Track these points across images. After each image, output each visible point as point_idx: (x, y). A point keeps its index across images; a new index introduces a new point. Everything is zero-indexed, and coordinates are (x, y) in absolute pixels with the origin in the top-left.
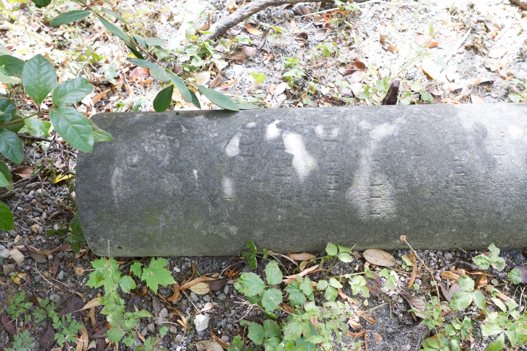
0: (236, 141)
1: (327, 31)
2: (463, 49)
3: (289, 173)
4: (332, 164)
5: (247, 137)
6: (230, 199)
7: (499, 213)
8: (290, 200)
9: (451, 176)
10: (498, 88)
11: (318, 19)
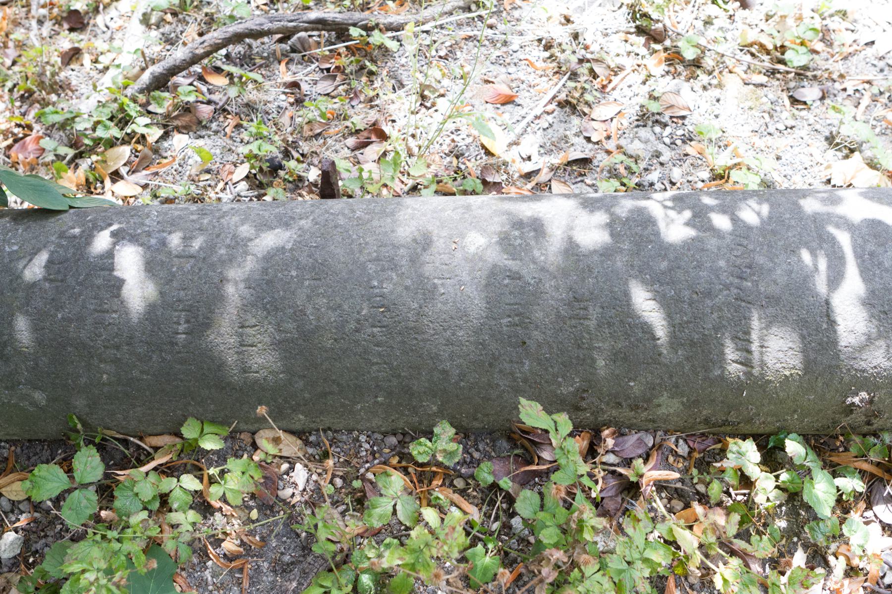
0: (43, 257)
2: (553, 106)
3: (115, 308)
4: (182, 293)
5: (61, 251)
6: (27, 348)
7: (445, 372)
8: (118, 350)
10: (598, 169)
11: (326, 59)
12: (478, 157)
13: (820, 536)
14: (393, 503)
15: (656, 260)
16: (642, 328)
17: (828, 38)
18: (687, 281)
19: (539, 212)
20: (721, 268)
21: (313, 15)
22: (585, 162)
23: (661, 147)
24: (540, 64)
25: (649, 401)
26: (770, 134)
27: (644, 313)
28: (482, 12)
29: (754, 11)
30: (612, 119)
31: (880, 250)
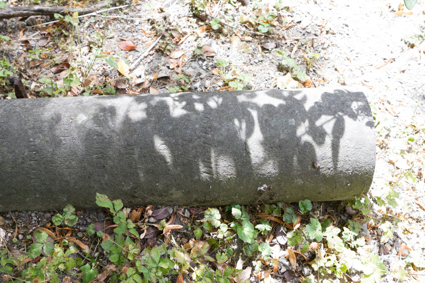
1: (49, 39)
7: (67, 181)
9: (26, 154)
12: (116, 76)
13: (250, 252)
14: (42, 246)
15: (167, 125)
16: (160, 158)
17: (280, 20)
18: (181, 135)
19: (115, 104)
20: (197, 128)
21: (36, 8)
22: (166, 78)
23: (201, 71)
24: (148, 32)
25: (167, 192)
26: (251, 64)
27: (160, 151)
28: (121, 7)
29: (248, 7)
30: (180, 57)
31: (270, 119)
